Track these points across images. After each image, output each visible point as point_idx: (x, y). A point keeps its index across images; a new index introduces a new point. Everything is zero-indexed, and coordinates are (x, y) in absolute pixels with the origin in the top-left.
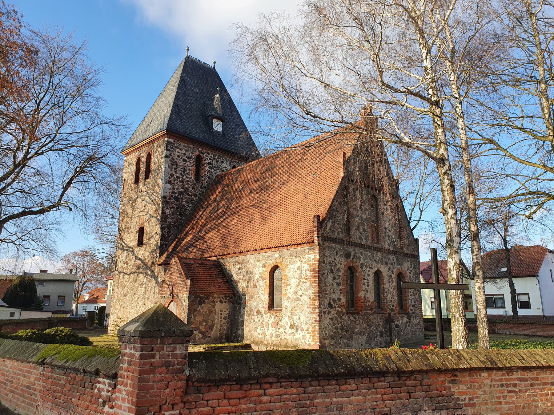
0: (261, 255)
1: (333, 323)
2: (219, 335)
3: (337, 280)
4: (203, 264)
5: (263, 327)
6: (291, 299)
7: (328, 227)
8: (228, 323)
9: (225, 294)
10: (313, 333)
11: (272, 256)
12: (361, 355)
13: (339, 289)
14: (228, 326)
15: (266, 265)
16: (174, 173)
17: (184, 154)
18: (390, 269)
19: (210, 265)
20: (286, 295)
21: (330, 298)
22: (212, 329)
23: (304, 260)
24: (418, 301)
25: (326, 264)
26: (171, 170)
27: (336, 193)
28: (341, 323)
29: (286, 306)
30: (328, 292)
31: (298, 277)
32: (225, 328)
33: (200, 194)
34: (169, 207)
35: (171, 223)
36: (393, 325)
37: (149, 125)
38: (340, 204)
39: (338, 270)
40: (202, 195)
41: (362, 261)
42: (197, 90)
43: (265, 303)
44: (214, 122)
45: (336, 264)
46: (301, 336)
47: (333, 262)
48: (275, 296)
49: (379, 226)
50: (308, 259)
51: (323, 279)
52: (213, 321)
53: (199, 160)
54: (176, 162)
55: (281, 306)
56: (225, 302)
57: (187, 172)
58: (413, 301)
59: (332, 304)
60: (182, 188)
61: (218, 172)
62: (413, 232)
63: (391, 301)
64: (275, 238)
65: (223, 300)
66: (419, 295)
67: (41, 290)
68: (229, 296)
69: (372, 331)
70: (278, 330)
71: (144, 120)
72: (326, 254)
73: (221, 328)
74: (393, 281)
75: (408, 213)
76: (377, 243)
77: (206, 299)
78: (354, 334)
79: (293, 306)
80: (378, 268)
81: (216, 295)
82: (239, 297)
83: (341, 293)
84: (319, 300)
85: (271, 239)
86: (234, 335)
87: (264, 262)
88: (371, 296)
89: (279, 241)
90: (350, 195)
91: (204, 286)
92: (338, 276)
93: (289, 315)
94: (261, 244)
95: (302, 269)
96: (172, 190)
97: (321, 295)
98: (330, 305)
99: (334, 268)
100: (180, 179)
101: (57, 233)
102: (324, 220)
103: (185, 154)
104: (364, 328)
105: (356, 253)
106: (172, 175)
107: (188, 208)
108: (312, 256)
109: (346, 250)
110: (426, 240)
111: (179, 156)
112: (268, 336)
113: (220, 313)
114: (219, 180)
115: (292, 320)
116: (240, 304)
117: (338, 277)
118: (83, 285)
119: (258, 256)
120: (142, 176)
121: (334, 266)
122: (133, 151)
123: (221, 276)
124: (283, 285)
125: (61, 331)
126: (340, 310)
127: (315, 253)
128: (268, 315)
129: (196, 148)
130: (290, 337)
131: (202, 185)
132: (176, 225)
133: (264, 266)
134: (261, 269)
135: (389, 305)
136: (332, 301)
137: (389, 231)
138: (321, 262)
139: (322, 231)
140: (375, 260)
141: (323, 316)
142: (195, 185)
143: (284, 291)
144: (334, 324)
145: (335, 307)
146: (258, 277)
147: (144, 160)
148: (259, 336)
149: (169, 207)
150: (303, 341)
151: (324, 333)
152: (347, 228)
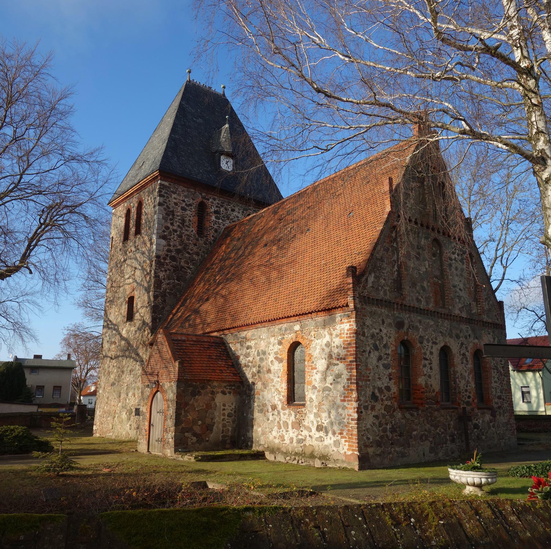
0: (276, 328)
1: (380, 423)
2: (221, 438)
3: (385, 360)
4: (199, 341)
5: (280, 428)
6: (318, 388)
7: (370, 284)
8: (234, 422)
9: (229, 381)
10: (349, 438)
11: (291, 329)
12: (380, 519)
13: (387, 373)
14: (234, 426)
15: (283, 341)
16: (169, 225)
17: (182, 200)
18: (462, 344)
19: (209, 342)
20: (310, 383)
21: (373, 386)
22: (211, 430)
23: (334, 333)
24: (506, 390)
25: (367, 337)
26: (166, 221)
27: (380, 235)
28: (391, 423)
29: (311, 398)
30: (370, 378)
32: (230, 429)
33: (203, 252)
34: (163, 269)
35: (166, 290)
36: (470, 425)
37: (141, 167)
38: (387, 250)
39: (385, 346)
40: (207, 253)
41: (421, 332)
42: (200, 120)
43: (282, 394)
44: (222, 160)
45: (382, 338)
46: (332, 442)
47: (378, 334)
48: (296, 385)
49: (446, 283)
50: (341, 331)
51: (363, 359)
52: (212, 419)
53: (202, 209)
54: (173, 211)
55: (303, 398)
56: (230, 393)
57: (187, 224)
58: (498, 391)
59: (378, 394)
60: (180, 245)
61: (227, 223)
62: (496, 294)
63: (466, 391)
64: (295, 303)
65: (227, 391)
66: (507, 382)
67: (31, 380)
68: (234, 385)
69: (438, 433)
70: (300, 433)
71: (135, 162)
72: (367, 323)
73: (224, 429)
74: (467, 361)
75: (488, 270)
76: (443, 307)
77: (202, 389)
78: (411, 438)
79: (320, 398)
80: (446, 342)
81: (215, 384)
82: (249, 385)
83: (390, 379)
84: (357, 389)
85: (289, 304)
86: (243, 438)
87: (280, 337)
88: (435, 383)
89: (300, 307)
90: (401, 239)
91: (199, 371)
92: (386, 354)
93: (315, 411)
94: (275, 312)
96: (167, 248)
97: (360, 383)
98: (374, 397)
99: (380, 343)
100: (178, 233)
101: (31, 307)
102: (363, 274)
103: (184, 201)
104: (426, 430)
105: (412, 321)
106: (167, 228)
107: (189, 271)
109: (398, 317)
110: (512, 308)
111: (176, 204)
112: (287, 441)
113: (222, 407)
114: (228, 232)
115: (319, 419)
116: (250, 396)
117: (386, 356)
118: (87, 373)
119: (272, 329)
121: (379, 340)
122: (123, 200)
123: (224, 358)
124: (306, 370)
125: (13, 430)
126: (389, 404)
127: (350, 322)
128: (287, 411)
129: (198, 193)
130: (318, 443)
131: (207, 240)
132: (172, 292)
133: (280, 343)
134: (277, 348)
135: (463, 396)
136: (376, 391)
137: (460, 290)
138: (360, 334)
139: (360, 289)
140: (441, 332)
141: (364, 413)
142: (197, 240)
143: (307, 378)
144: (380, 425)
145: (382, 400)
146: (273, 359)
147: (134, 211)
148: (275, 440)
149: (163, 269)
150: (335, 449)
151: (365, 438)
152: (398, 286)
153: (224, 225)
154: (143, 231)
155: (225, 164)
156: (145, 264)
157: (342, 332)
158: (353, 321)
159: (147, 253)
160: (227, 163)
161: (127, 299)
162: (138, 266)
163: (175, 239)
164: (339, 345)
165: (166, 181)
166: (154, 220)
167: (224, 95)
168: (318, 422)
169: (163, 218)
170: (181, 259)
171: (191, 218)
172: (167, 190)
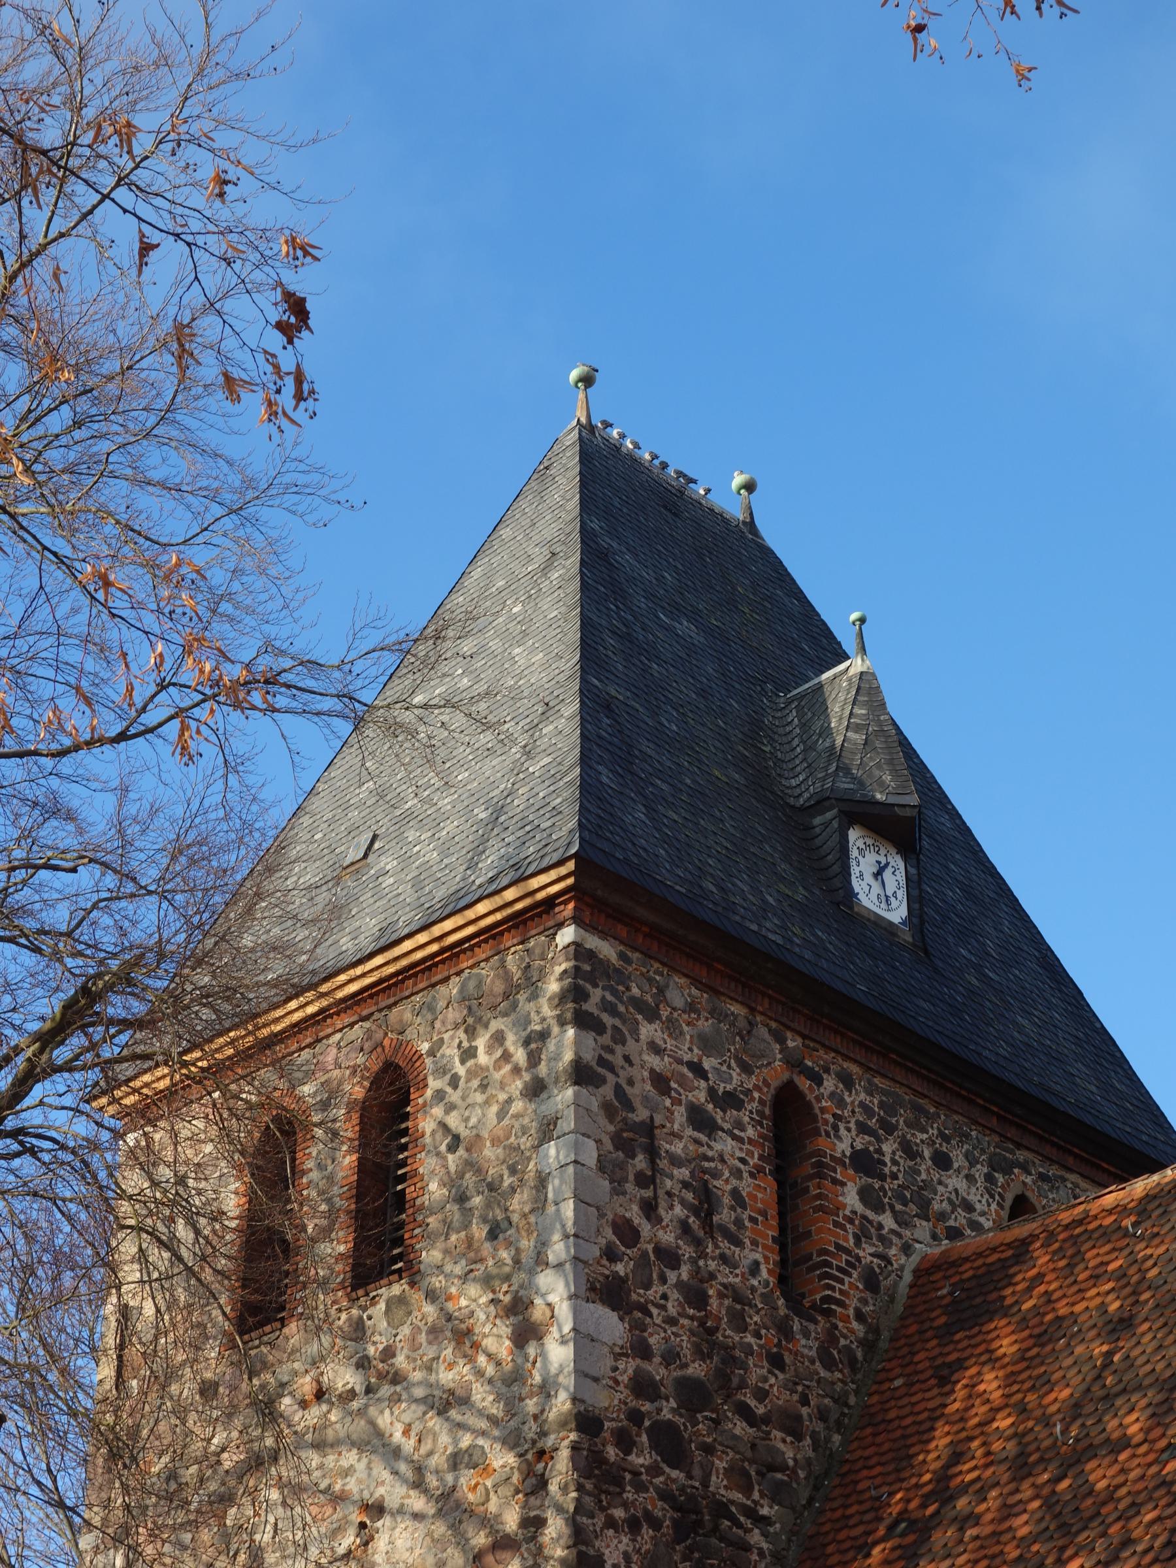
16: (635, 1214)
26: (618, 1189)
54: (649, 1129)
60: (700, 1354)
103: (698, 1070)
111: (660, 1082)
129: (763, 1032)
131: (831, 1337)
142: (784, 1330)
149: (619, 1513)
153: (907, 1249)
154: (430, 1256)
155: (869, 878)
156: (466, 1478)
159: (482, 1396)
160: (878, 874)
162: (392, 1491)
163: (672, 1310)
165: (604, 935)
166: (542, 1181)
167: (751, 525)
169: (601, 1167)
170: (708, 1449)
171: (746, 1185)
172: (614, 993)
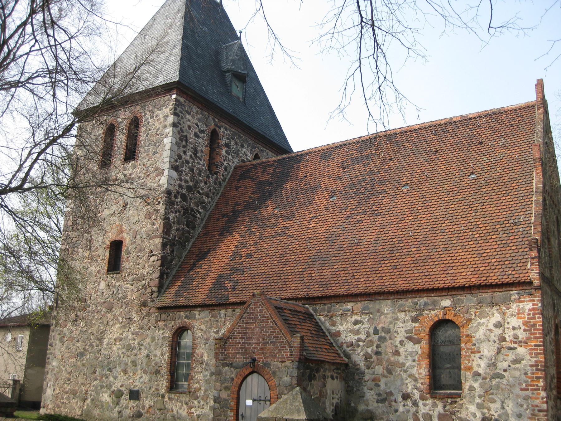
26: (179, 146)
31: (496, 339)
35: (175, 237)
53: (214, 136)
55: (458, 386)
56: (337, 378)
60: (191, 181)
95: (506, 326)
107: (198, 216)
108: (528, 306)
111: (189, 127)
120: (119, 152)
124: (463, 352)
127: (534, 301)
129: (211, 118)
142: (208, 177)
143: (464, 363)
157: (521, 311)
158: (538, 300)
161: (108, 243)
164: (516, 326)
165: (182, 97)
168: (483, 414)
169: (176, 143)
170: (191, 199)
172: (182, 109)
